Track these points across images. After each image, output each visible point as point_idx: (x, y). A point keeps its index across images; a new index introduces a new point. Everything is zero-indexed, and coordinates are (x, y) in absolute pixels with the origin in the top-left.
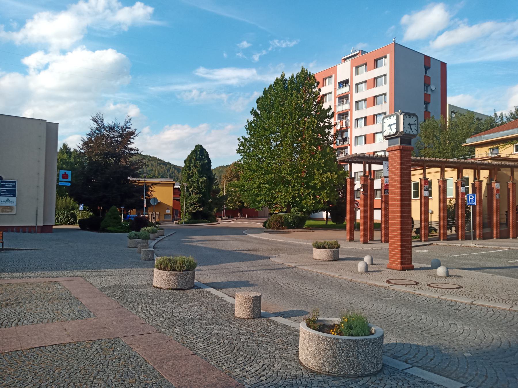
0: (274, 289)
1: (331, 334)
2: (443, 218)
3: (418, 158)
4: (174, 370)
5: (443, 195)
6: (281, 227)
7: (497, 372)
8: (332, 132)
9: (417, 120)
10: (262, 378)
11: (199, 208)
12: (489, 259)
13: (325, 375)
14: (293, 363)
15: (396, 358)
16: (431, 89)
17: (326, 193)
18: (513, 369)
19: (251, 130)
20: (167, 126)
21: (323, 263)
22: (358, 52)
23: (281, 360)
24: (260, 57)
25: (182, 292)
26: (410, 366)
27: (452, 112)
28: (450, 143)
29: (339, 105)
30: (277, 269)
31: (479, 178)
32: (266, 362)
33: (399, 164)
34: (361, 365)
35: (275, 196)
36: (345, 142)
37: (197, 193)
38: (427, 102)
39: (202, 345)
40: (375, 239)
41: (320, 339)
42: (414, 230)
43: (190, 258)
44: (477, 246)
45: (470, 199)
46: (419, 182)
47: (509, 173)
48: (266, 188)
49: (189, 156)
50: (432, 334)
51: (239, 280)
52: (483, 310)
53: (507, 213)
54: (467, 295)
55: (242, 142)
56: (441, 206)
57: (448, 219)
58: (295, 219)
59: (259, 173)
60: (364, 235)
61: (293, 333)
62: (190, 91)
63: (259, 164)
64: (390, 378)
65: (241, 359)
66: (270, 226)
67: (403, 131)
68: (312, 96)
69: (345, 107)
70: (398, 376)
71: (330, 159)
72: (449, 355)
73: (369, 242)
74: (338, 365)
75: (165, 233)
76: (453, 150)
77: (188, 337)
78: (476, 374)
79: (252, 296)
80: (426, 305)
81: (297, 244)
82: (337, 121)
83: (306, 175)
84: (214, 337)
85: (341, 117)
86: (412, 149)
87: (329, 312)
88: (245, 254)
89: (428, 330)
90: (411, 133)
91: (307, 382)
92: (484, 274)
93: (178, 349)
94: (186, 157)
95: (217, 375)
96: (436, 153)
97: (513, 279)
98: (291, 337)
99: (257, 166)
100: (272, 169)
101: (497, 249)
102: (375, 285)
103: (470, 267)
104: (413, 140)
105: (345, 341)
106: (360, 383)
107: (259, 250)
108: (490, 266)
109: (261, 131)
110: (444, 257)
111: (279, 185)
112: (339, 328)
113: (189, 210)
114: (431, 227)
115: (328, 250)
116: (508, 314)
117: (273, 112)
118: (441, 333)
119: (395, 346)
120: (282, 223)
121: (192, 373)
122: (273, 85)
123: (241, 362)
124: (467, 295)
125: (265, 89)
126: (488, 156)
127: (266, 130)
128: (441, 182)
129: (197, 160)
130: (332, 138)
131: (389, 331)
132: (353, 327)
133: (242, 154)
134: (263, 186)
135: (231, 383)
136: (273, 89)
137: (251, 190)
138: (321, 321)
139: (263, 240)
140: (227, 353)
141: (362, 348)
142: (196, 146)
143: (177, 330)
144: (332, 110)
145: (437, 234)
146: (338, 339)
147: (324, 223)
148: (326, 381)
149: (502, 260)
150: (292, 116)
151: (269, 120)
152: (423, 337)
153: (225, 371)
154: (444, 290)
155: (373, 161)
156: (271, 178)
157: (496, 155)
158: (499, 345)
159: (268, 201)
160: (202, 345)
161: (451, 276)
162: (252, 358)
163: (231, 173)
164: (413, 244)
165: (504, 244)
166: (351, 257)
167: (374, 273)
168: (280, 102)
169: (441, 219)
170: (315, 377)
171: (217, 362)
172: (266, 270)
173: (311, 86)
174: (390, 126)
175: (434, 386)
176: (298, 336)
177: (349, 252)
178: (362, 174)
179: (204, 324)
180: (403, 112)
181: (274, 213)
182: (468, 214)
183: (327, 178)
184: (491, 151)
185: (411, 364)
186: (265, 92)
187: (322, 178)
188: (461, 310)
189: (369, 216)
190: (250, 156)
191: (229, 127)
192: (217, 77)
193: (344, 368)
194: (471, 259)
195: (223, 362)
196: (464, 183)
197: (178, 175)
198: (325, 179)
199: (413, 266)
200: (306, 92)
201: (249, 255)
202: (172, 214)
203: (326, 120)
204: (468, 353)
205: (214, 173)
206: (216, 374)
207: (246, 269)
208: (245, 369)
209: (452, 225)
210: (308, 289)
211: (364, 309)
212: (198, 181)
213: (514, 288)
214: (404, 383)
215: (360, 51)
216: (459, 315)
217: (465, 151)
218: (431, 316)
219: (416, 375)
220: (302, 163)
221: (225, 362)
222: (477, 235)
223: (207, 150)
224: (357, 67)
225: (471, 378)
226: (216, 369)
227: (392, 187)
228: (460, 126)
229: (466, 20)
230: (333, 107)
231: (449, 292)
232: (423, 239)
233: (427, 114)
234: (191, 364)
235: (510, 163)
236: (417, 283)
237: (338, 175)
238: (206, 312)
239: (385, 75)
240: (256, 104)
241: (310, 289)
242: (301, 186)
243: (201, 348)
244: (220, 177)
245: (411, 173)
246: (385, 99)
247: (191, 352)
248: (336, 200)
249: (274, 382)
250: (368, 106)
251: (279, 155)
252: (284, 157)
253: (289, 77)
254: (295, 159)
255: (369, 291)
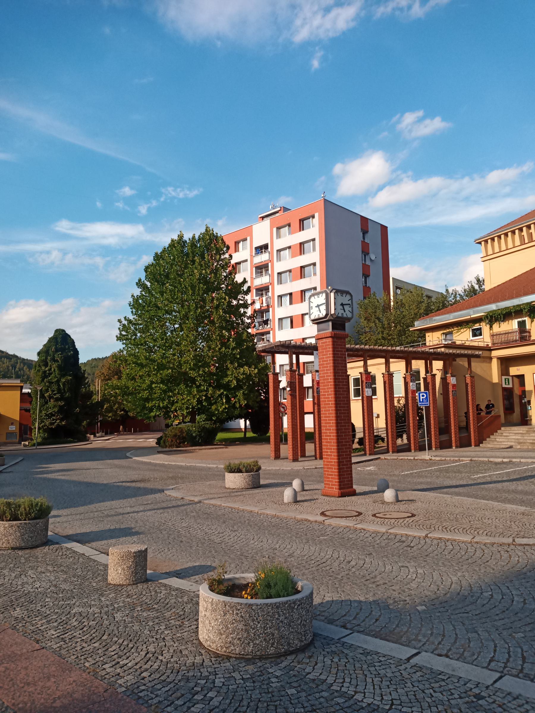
0: (168, 537)
1: (243, 598)
2: (391, 423)
3: (357, 346)
4: (7, 678)
5: (390, 394)
6: (181, 445)
7: (456, 627)
8: (249, 312)
9: (351, 299)
10: (144, 674)
11: (60, 422)
12: (448, 475)
13: (234, 659)
14: (190, 645)
15: (331, 622)
16: (371, 259)
17: (243, 393)
18: (474, 622)
19: (137, 309)
20: (12, 302)
21: (239, 493)
22: (279, 209)
23: (173, 643)
24: (149, 209)
25: (28, 551)
26: (349, 632)
27: (397, 288)
28: (395, 327)
29: (256, 277)
30: (173, 507)
31: (432, 371)
32: (151, 649)
33: (331, 355)
34: (283, 638)
35: (173, 401)
36: (266, 326)
37: (57, 400)
38: (366, 275)
39: (54, 633)
40: (307, 454)
41: (227, 607)
42: (356, 440)
43: (41, 500)
44: (433, 458)
45: (421, 398)
46: (360, 377)
47: (466, 365)
48: (160, 389)
49: (45, 345)
50: (378, 584)
51: (118, 526)
52: (440, 545)
53: (467, 414)
54: (421, 526)
55: (124, 325)
56: (388, 408)
57: (397, 424)
58: (201, 431)
59: (150, 368)
60: (293, 450)
61: (192, 600)
62: (48, 252)
63: (150, 356)
64: (323, 653)
65: (114, 647)
66: (167, 444)
67: (335, 313)
68: (220, 265)
69: (264, 280)
70: (334, 648)
71: (248, 347)
72: (399, 611)
73: (300, 459)
74: (253, 642)
75: (6, 461)
76: (400, 334)
77: (34, 622)
78: (432, 634)
79: (133, 551)
80: (370, 543)
81: (204, 467)
82: (255, 298)
83: (216, 370)
84: (75, 619)
85: (260, 293)
86: (347, 336)
87: (244, 565)
88: (129, 487)
89: (373, 578)
90: (345, 316)
91: (209, 673)
92: (441, 495)
93: (16, 644)
94: (41, 347)
95: (75, 678)
96: (380, 339)
97: (476, 500)
98: (189, 606)
99: (146, 359)
100: (169, 362)
101: (456, 461)
102: (306, 520)
103: (425, 487)
104: (347, 324)
105: (261, 607)
106: (283, 665)
107: (149, 481)
108: (449, 485)
109: (151, 310)
110: (394, 475)
111: (178, 385)
112: (253, 589)
113: (45, 425)
114: (377, 436)
115: (245, 474)
116: (469, 548)
117: (168, 285)
118: (389, 581)
119: (331, 606)
120: (184, 438)
121: (36, 679)
122: (168, 248)
123: (113, 653)
124: (421, 526)
125: (156, 254)
126: (440, 343)
127: (159, 309)
128: (386, 376)
129: (57, 350)
130: (249, 321)
131: (322, 584)
132: (272, 585)
133: (125, 342)
134: (156, 387)
135: (96, 687)
136: (167, 254)
137: (139, 393)
138: (229, 580)
139: (156, 465)
140: (93, 641)
141: (284, 614)
142: (57, 331)
143: (18, 612)
144: (249, 284)
145: (385, 444)
146: (252, 605)
147: (241, 435)
148: (236, 667)
149: (463, 475)
150: (194, 291)
151: (162, 295)
152: (367, 589)
153: (88, 671)
154: (393, 521)
155: (301, 351)
156: (167, 375)
157: (450, 342)
158: (458, 591)
159: (163, 407)
160: (54, 633)
161: (401, 501)
162: (131, 645)
163: (109, 369)
164: (354, 460)
165: (465, 454)
166: (276, 481)
167: (306, 504)
168: (178, 271)
169: (389, 425)
170: (220, 663)
171: (78, 657)
172: (157, 509)
173: (219, 252)
174: (318, 306)
175: (380, 657)
176: (198, 604)
177: (275, 474)
178: (287, 368)
179: (61, 599)
180: (333, 289)
181: (172, 425)
182: (421, 418)
183: (243, 374)
184: (444, 337)
185: (351, 629)
186: (157, 257)
187: (238, 374)
188: (413, 547)
189: (298, 424)
190: (136, 345)
191: (107, 303)
192: (88, 234)
193: (260, 645)
194: (426, 477)
195: (86, 656)
196: (414, 378)
197: (28, 373)
198: (241, 375)
199: (355, 491)
200: (212, 259)
201: (135, 488)
202: (18, 431)
203: (240, 297)
204: (422, 605)
205: (83, 368)
206: (74, 676)
207: (129, 509)
208: (118, 663)
209: (402, 431)
210: (217, 532)
211: (291, 555)
212: (58, 381)
213: (477, 512)
214: (341, 657)
215: (281, 208)
216: (412, 554)
217: (415, 337)
218: (376, 558)
219: (357, 644)
220: (210, 354)
221: (90, 655)
222: (433, 444)
223: (72, 337)
224: (279, 228)
225: (425, 640)
226: (74, 669)
227: (324, 386)
228: (407, 305)
229: (410, 173)
230: (248, 279)
231: (399, 524)
232: (368, 452)
233: (366, 290)
234: (35, 666)
235: (466, 352)
236: (360, 514)
237: (259, 370)
238: (65, 581)
239: (314, 240)
240: (144, 274)
241: (219, 533)
242: (210, 385)
243: (53, 637)
244: (94, 374)
245: (346, 367)
246: (315, 270)
247: (37, 646)
248: (257, 402)
249: (162, 678)
250: (293, 279)
251: (178, 343)
252: (184, 346)
253: (190, 239)
254: (200, 348)
255: (299, 529)
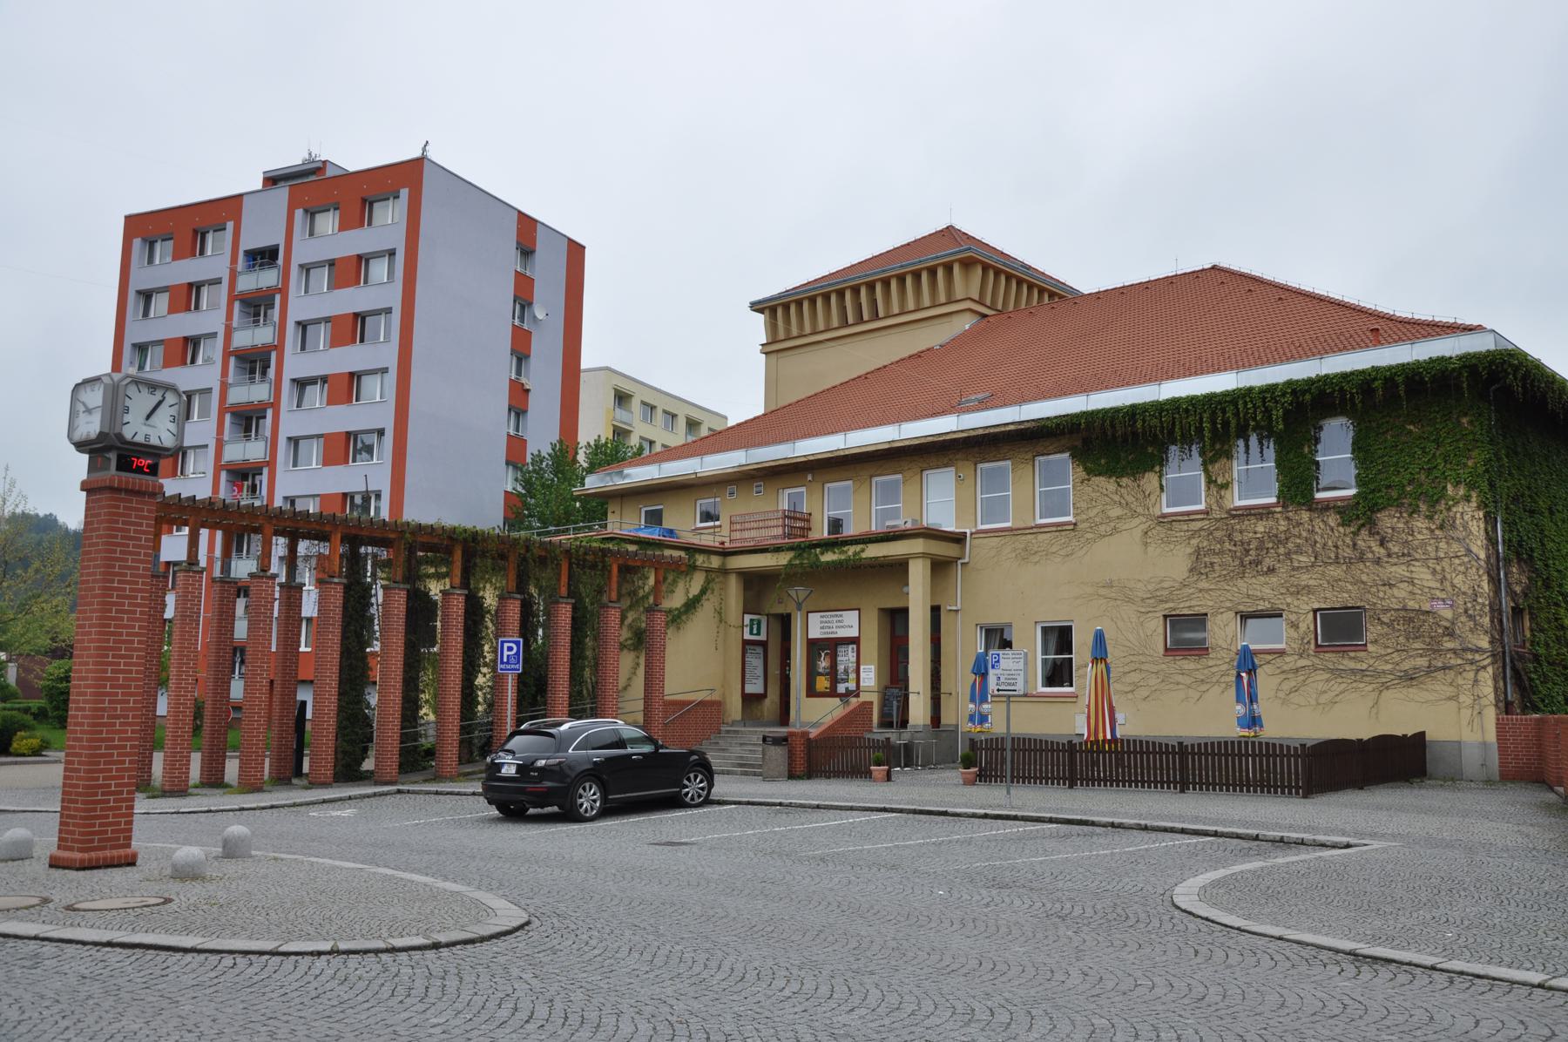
45: (506, 653)
